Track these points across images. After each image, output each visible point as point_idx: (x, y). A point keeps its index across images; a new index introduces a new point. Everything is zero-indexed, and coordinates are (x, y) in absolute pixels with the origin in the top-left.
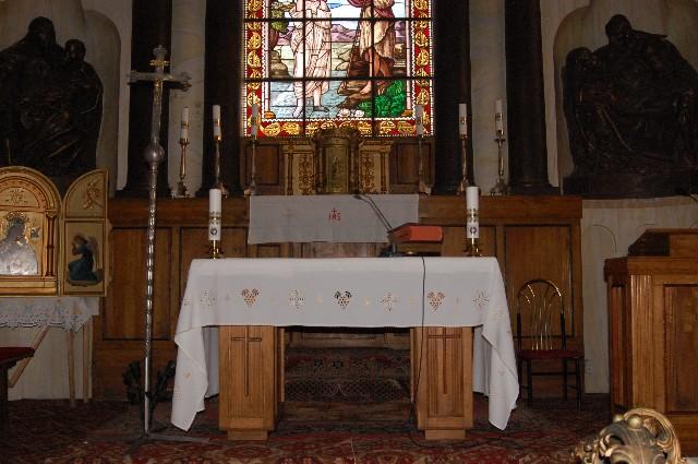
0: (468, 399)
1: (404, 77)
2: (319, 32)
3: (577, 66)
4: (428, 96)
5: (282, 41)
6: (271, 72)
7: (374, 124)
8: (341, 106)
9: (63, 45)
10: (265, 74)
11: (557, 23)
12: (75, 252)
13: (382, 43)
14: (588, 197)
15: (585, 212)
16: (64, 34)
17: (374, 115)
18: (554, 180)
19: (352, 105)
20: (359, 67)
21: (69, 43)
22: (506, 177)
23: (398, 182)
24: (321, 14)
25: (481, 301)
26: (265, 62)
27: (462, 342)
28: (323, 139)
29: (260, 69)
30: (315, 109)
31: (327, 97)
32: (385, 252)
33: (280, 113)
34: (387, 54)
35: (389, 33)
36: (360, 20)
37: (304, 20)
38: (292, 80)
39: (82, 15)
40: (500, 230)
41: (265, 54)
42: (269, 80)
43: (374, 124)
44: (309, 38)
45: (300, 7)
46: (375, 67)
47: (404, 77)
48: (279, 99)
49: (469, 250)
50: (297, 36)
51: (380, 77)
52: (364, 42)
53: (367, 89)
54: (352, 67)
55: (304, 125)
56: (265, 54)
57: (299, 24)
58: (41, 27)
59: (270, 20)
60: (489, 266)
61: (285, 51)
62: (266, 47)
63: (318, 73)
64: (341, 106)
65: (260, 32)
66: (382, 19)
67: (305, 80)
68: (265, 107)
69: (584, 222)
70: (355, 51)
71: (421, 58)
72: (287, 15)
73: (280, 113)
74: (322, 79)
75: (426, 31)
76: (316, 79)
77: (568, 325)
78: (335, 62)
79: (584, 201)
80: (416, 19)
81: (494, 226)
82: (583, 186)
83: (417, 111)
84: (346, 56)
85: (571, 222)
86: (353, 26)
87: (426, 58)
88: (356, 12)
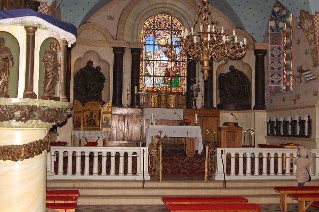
0: (195, 151)
1: (179, 76)
2: (158, 64)
3: (221, 77)
4: (185, 82)
5: (148, 66)
6: (145, 74)
7: (171, 88)
8: (163, 83)
9: (95, 68)
10: (144, 74)
11: (217, 67)
12: (105, 120)
13: (174, 67)
14: (222, 110)
15: (221, 113)
16: (95, 65)
17: (171, 86)
18: (215, 105)
19: (165, 83)
20: (168, 74)
21: (97, 68)
22: (203, 105)
23: (177, 106)
24: (158, 59)
25: (197, 133)
26: (144, 71)
27: (192, 140)
28: (159, 93)
29: (142, 73)
30: (156, 84)
31: (159, 81)
32: (181, 124)
33: (147, 85)
34: (175, 70)
35: (175, 65)
36: (168, 61)
37: (154, 60)
38: (150, 76)
39: (100, 60)
40: (202, 118)
41: (144, 70)
42: (145, 76)
43: (171, 88)
44: (155, 65)
45: (153, 57)
46: (172, 73)
47: (179, 76)
48: (147, 81)
49: (195, 125)
50: (152, 65)
51: (173, 76)
52: (169, 67)
53: (170, 79)
54: (165, 74)
55: (153, 88)
56: (144, 70)
57: (152, 62)
58: (90, 63)
59: (145, 60)
60: (199, 127)
61: (149, 69)
62: (144, 67)
63: (157, 75)
64: (163, 83)
65: (142, 63)
66: (174, 61)
67: (154, 76)
68: (143, 83)
69: (221, 116)
70: (167, 69)
71: (183, 72)
72: (149, 59)
73: (147, 85)
74: (158, 76)
75: (185, 65)
76: (156, 76)
77: (216, 140)
78: (160, 71)
79: (221, 111)
80: (183, 61)
81: (200, 117)
82: (221, 107)
83: (182, 86)
84: (164, 71)
85: (218, 116)
86: (166, 62)
87: (185, 71)
88: (167, 59)
